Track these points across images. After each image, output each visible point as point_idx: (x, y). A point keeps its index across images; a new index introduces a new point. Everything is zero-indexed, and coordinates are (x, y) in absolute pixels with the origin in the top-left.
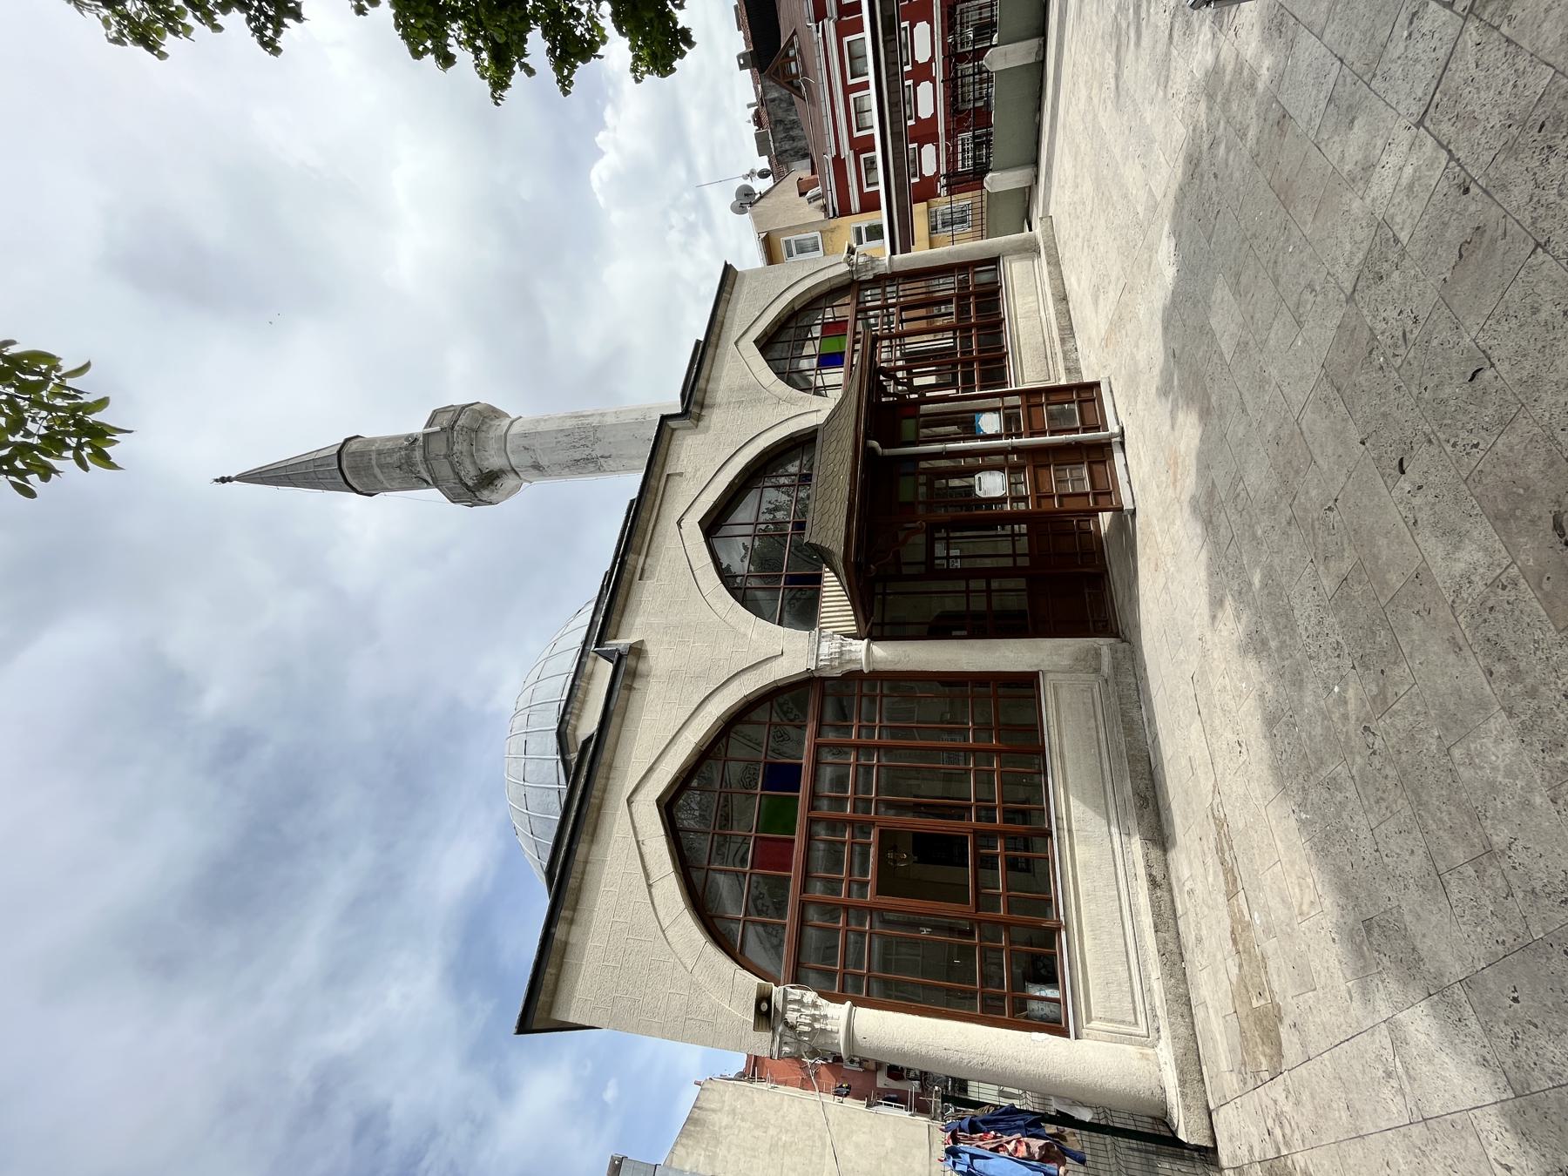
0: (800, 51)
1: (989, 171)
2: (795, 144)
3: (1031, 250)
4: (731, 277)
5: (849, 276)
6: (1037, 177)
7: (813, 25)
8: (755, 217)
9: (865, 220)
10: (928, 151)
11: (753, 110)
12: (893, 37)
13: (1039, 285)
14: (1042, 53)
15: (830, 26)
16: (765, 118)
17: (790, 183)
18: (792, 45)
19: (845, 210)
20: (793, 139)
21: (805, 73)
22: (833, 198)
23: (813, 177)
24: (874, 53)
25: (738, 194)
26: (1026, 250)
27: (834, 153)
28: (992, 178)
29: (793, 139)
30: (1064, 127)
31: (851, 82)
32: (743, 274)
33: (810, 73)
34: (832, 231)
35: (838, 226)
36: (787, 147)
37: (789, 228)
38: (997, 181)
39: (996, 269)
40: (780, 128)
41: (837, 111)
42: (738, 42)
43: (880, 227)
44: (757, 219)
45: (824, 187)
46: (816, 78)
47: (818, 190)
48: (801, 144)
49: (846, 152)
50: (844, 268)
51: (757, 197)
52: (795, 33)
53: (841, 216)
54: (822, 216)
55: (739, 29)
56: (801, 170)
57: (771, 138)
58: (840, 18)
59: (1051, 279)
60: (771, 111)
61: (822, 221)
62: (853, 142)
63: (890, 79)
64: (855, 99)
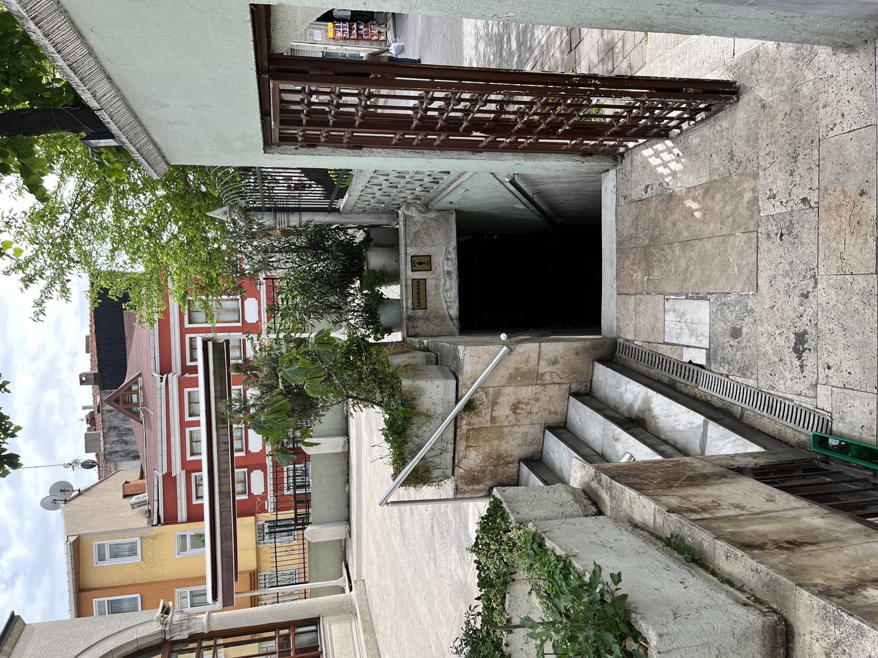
0: (142, 388)
1: (308, 523)
2: (127, 447)
3: (347, 611)
4: (14, 632)
5: (161, 636)
6: (350, 532)
7: (158, 376)
8: (67, 516)
9: (192, 529)
10: (257, 476)
11: (88, 411)
12: (226, 425)
13: (357, 652)
14: (347, 447)
15: (173, 380)
16: (98, 418)
17: (116, 482)
18: (136, 383)
19: (170, 518)
20: (126, 443)
21: (145, 404)
22: (159, 507)
23: (141, 481)
24: (211, 530)
25: (52, 489)
26: (344, 611)
27: (165, 471)
28: (312, 531)
29: (126, 443)
30: (368, 518)
31: (188, 419)
32: (33, 627)
33: (150, 405)
34: (154, 537)
35: (161, 534)
36: (118, 449)
37: (105, 533)
38: (315, 533)
39: (316, 631)
40: (113, 433)
41: (172, 439)
42: (85, 363)
43: (202, 536)
44: (69, 520)
45: (151, 495)
46: (155, 412)
47: (144, 497)
48: (131, 448)
49: (178, 471)
50: (156, 627)
51: (74, 494)
52: (140, 375)
53: (165, 524)
54: (144, 522)
55: (87, 352)
56: (129, 471)
57: (102, 439)
58: (183, 374)
59: (368, 649)
60: (106, 418)
61: (144, 528)
62: (185, 464)
63: (222, 510)
64: (189, 393)
